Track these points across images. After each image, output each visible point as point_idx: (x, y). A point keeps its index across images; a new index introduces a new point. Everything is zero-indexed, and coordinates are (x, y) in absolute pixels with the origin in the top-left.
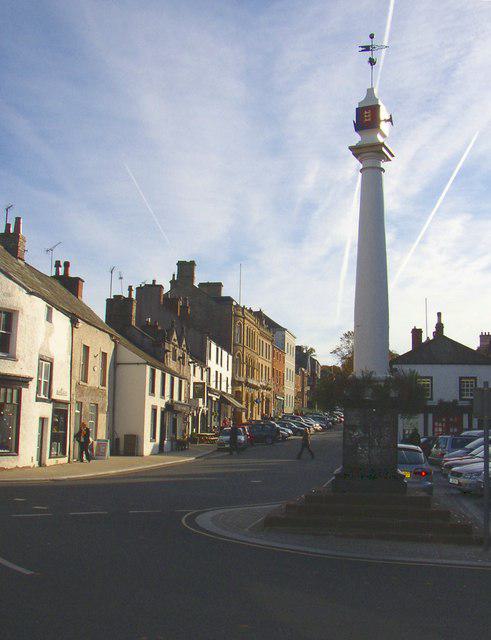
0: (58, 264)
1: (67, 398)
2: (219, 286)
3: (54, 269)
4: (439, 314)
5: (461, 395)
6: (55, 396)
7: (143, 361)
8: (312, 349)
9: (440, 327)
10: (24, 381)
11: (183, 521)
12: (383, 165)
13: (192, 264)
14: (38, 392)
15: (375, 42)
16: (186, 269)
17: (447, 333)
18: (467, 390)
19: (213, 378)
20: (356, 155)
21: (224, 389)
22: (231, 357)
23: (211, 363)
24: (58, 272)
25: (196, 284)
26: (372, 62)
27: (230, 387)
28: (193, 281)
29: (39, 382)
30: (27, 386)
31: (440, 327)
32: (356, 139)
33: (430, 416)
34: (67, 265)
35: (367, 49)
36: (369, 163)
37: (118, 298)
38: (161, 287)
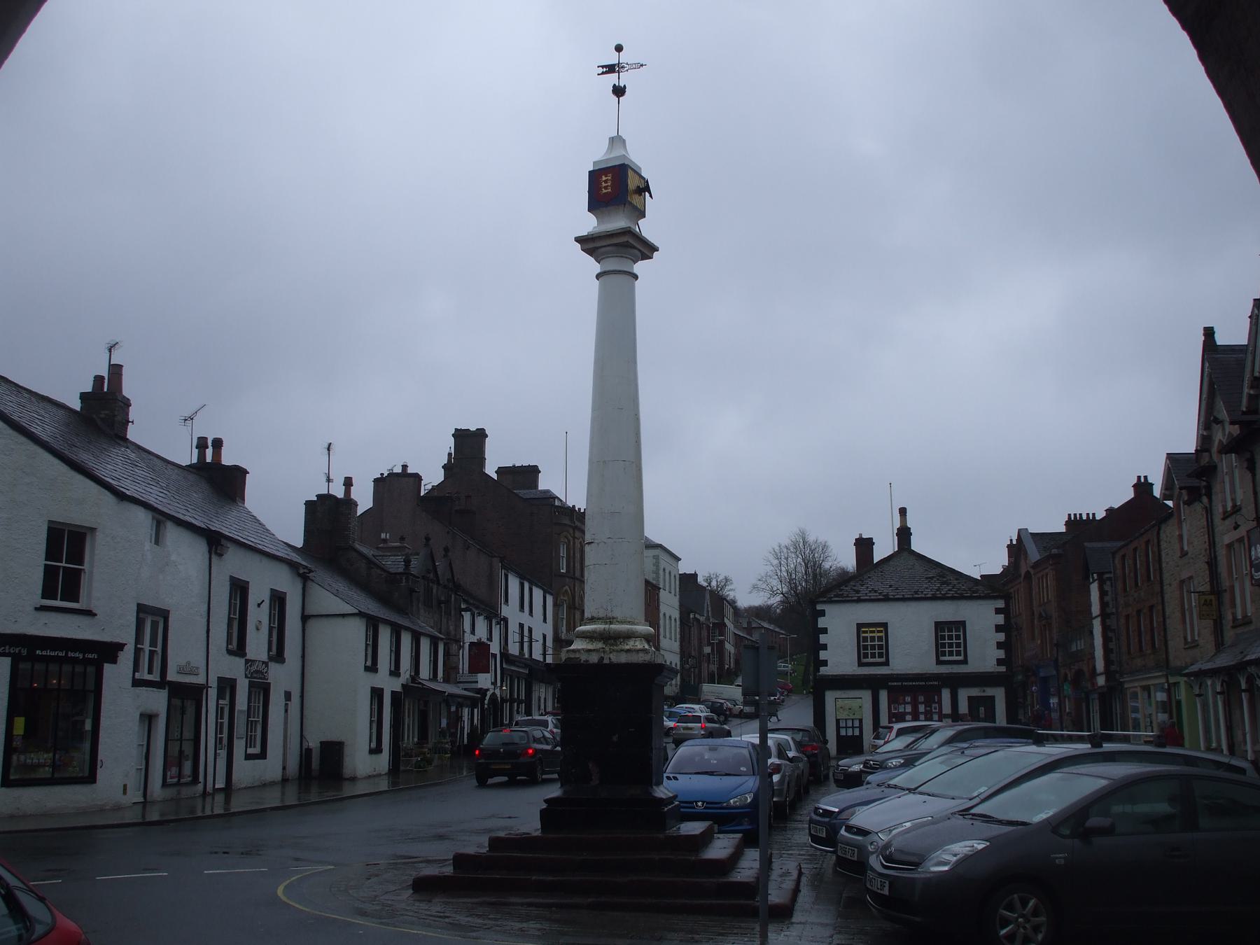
0: (202, 444)
1: (200, 680)
2: (533, 471)
3: (196, 451)
4: (903, 512)
5: (939, 653)
6: (172, 676)
7: (348, 609)
8: (727, 579)
9: (904, 534)
10: (110, 651)
11: (280, 891)
12: (640, 267)
13: (481, 435)
14: (136, 668)
15: (625, 57)
16: (469, 444)
17: (918, 545)
18: (950, 637)
19: (514, 637)
20: (590, 252)
21: (537, 655)
22: (550, 599)
23: (510, 611)
24: (202, 455)
25: (491, 470)
26: (619, 91)
27: (550, 651)
28: (482, 460)
29: (138, 652)
30: (114, 661)
31: (904, 534)
32: (589, 224)
33: (883, 696)
34: (218, 444)
35: (610, 69)
36: (612, 264)
37: (325, 499)
38: (417, 478)
